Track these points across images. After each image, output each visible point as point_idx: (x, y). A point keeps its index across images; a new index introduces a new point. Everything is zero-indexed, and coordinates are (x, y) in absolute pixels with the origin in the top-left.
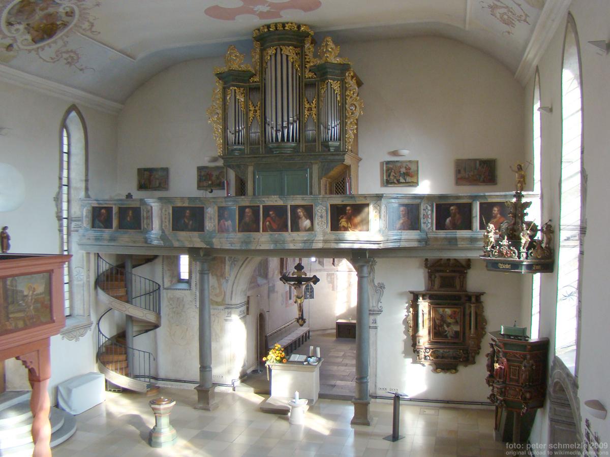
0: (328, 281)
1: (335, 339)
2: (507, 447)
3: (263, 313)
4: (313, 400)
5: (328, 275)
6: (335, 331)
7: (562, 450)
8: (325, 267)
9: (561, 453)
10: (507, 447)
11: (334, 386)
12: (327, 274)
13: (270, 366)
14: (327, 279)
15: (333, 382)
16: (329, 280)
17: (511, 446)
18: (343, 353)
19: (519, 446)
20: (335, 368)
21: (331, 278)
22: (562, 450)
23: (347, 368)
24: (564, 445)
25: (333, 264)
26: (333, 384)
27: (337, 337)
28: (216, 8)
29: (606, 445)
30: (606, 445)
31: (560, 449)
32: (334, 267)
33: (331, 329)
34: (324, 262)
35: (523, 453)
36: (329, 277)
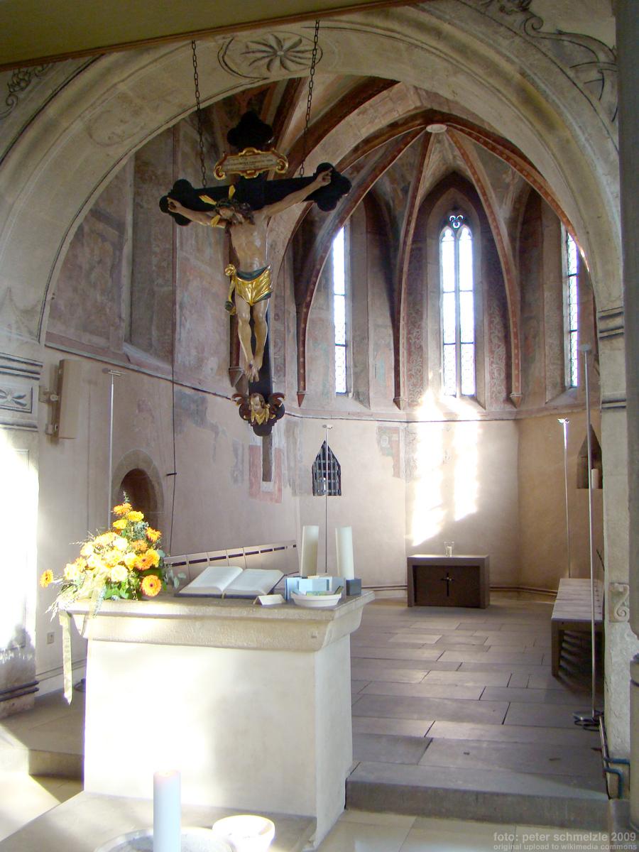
0: (382, 449)
1: (405, 607)
2: (495, 839)
3: (142, 466)
4: (310, 822)
5: (381, 431)
6: (402, 594)
7: (573, 843)
8: (373, 409)
9: (571, 847)
10: (495, 839)
11: (426, 743)
12: (379, 428)
13: (79, 620)
14: (379, 442)
15: (418, 727)
16: (385, 444)
17: (501, 837)
18: (437, 638)
19: (511, 837)
20: (419, 675)
21: (390, 441)
22: (573, 843)
23: (459, 675)
24: (574, 836)
25: (397, 402)
26: (420, 733)
27: (410, 605)
28: (242, 415)
29: (633, 835)
30: (633, 835)
31: (569, 842)
32: (401, 412)
33: (393, 588)
34: (371, 394)
35: (517, 847)
36: (385, 437)
